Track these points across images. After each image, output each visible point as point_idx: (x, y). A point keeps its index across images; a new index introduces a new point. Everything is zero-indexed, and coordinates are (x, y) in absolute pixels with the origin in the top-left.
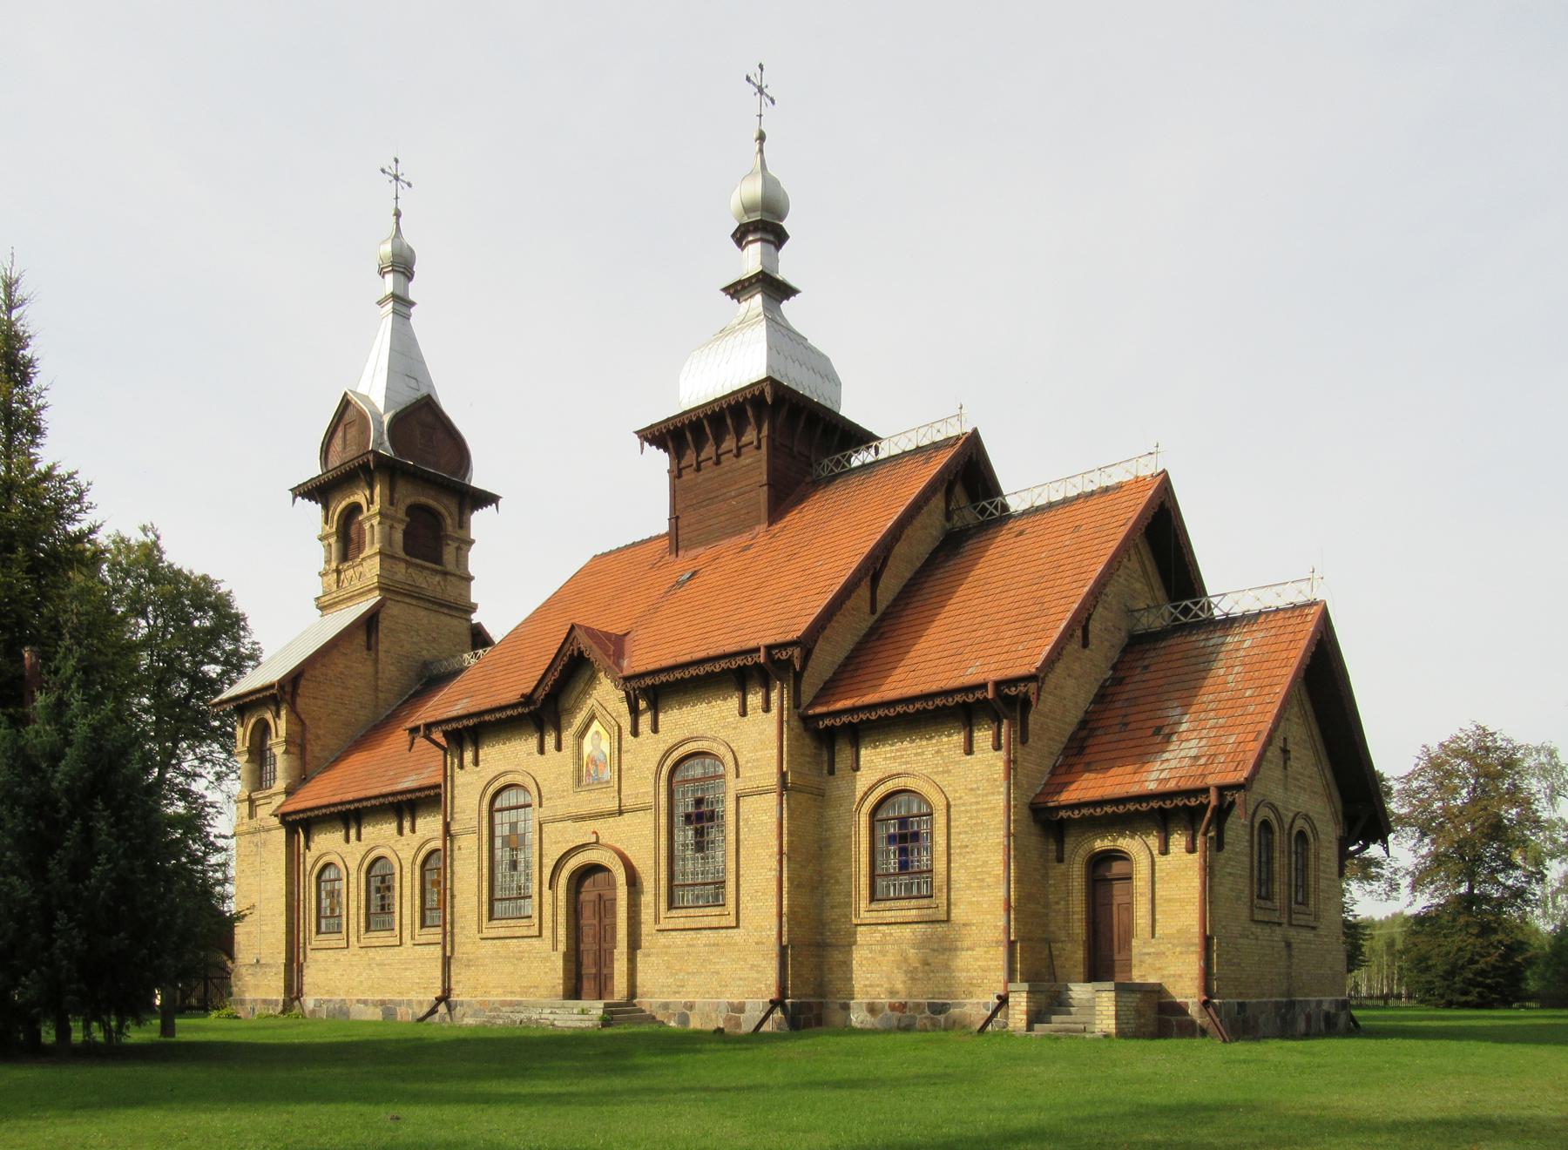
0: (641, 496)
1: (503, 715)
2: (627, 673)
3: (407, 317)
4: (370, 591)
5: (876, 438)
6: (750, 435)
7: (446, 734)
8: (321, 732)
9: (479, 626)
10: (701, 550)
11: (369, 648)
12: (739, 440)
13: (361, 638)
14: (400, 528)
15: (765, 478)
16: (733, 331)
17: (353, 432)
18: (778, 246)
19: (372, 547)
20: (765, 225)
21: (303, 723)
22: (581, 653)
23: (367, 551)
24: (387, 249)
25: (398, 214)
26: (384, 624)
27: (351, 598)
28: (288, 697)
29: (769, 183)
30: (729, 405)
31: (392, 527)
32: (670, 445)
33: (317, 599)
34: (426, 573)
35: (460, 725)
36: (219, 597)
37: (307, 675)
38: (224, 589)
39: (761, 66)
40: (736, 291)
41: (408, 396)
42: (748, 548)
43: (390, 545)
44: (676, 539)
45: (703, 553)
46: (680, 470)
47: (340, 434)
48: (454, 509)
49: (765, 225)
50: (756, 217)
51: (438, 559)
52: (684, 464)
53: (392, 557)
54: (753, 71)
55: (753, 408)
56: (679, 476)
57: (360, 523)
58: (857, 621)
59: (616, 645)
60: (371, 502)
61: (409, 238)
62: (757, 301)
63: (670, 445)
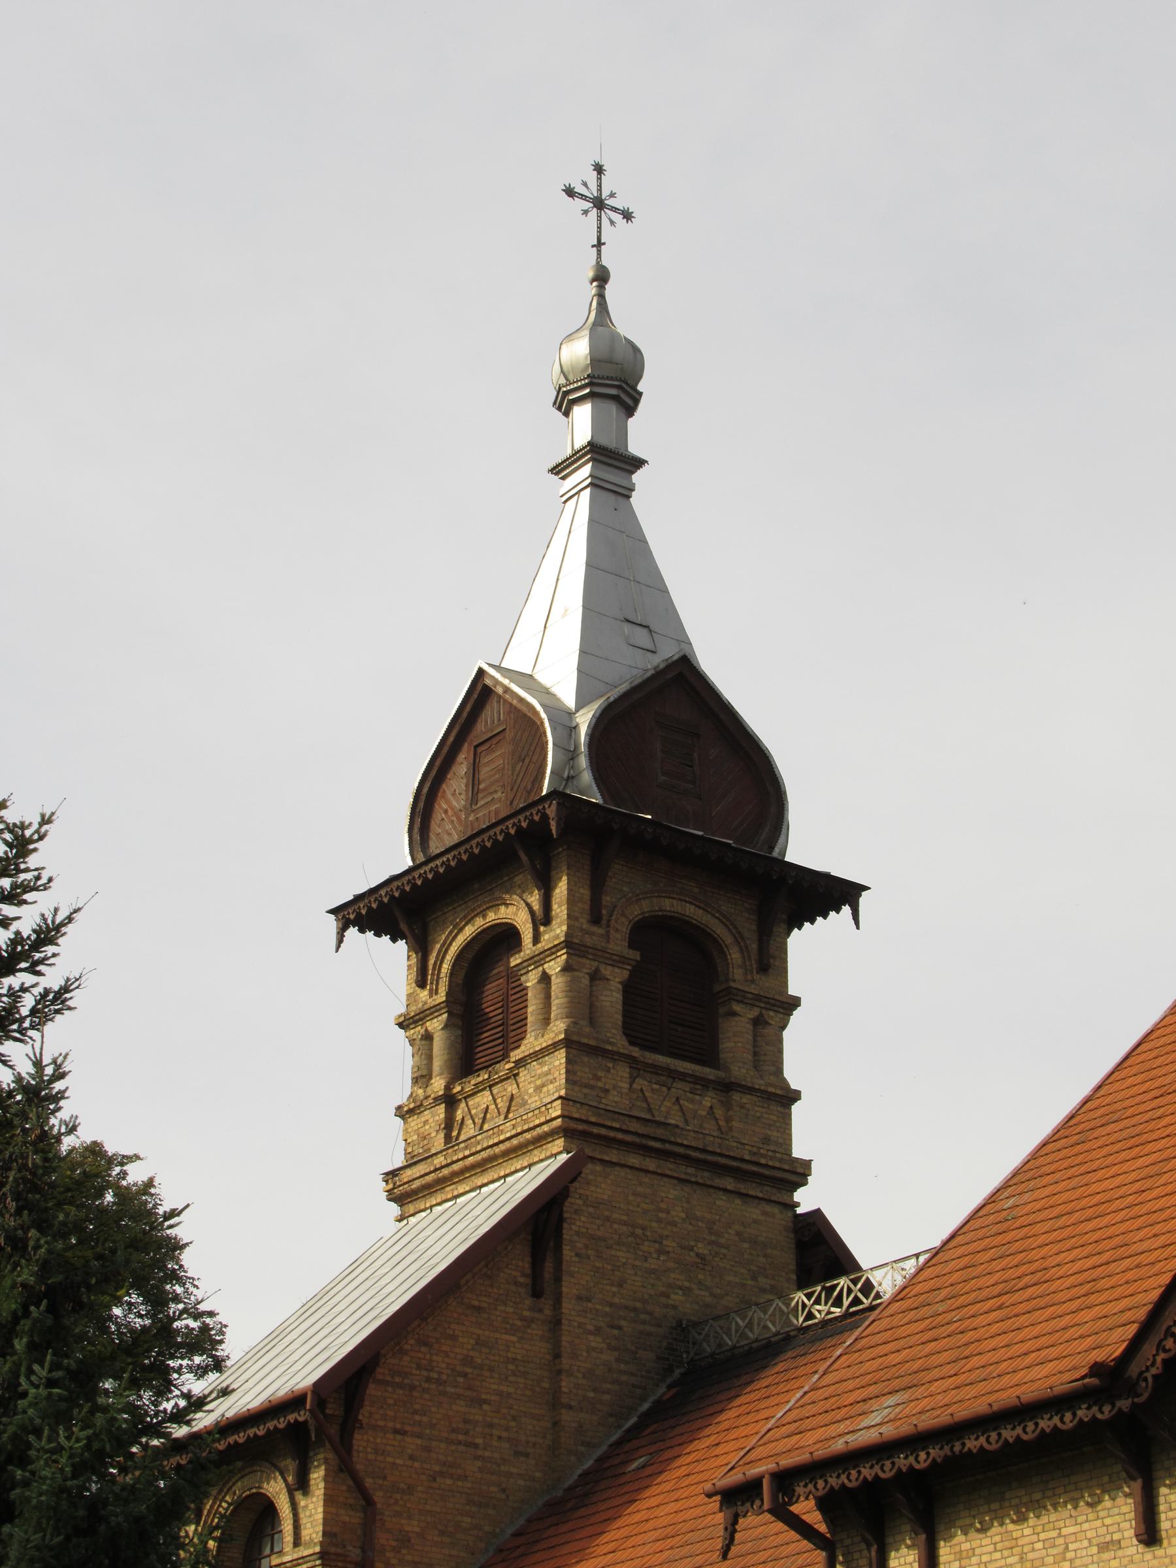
1: (1028, 1431)
3: (625, 493)
4: (540, 1141)
7: (824, 1504)
8: (413, 1526)
9: (817, 1216)
11: (537, 1293)
13: (517, 1265)
14: (616, 976)
17: (495, 762)
18: (630, 410)
19: (544, 1032)
21: (369, 1502)
23: (532, 1042)
24: (579, 350)
25: (601, 277)
26: (577, 1224)
27: (482, 1166)
28: (333, 1430)
31: (595, 976)
32: (403, 927)
33: (390, 1175)
34: (679, 1087)
35: (886, 1470)
36: (125, 1195)
37: (381, 1372)
38: (135, 1175)
41: (632, 666)
43: (592, 1021)
47: (461, 768)
48: (749, 928)
51: (708, 1054)
53: (597, 1051)
57: (514, 976)
60: (543, 919)
61: (625, 324)
63: (403, 927)
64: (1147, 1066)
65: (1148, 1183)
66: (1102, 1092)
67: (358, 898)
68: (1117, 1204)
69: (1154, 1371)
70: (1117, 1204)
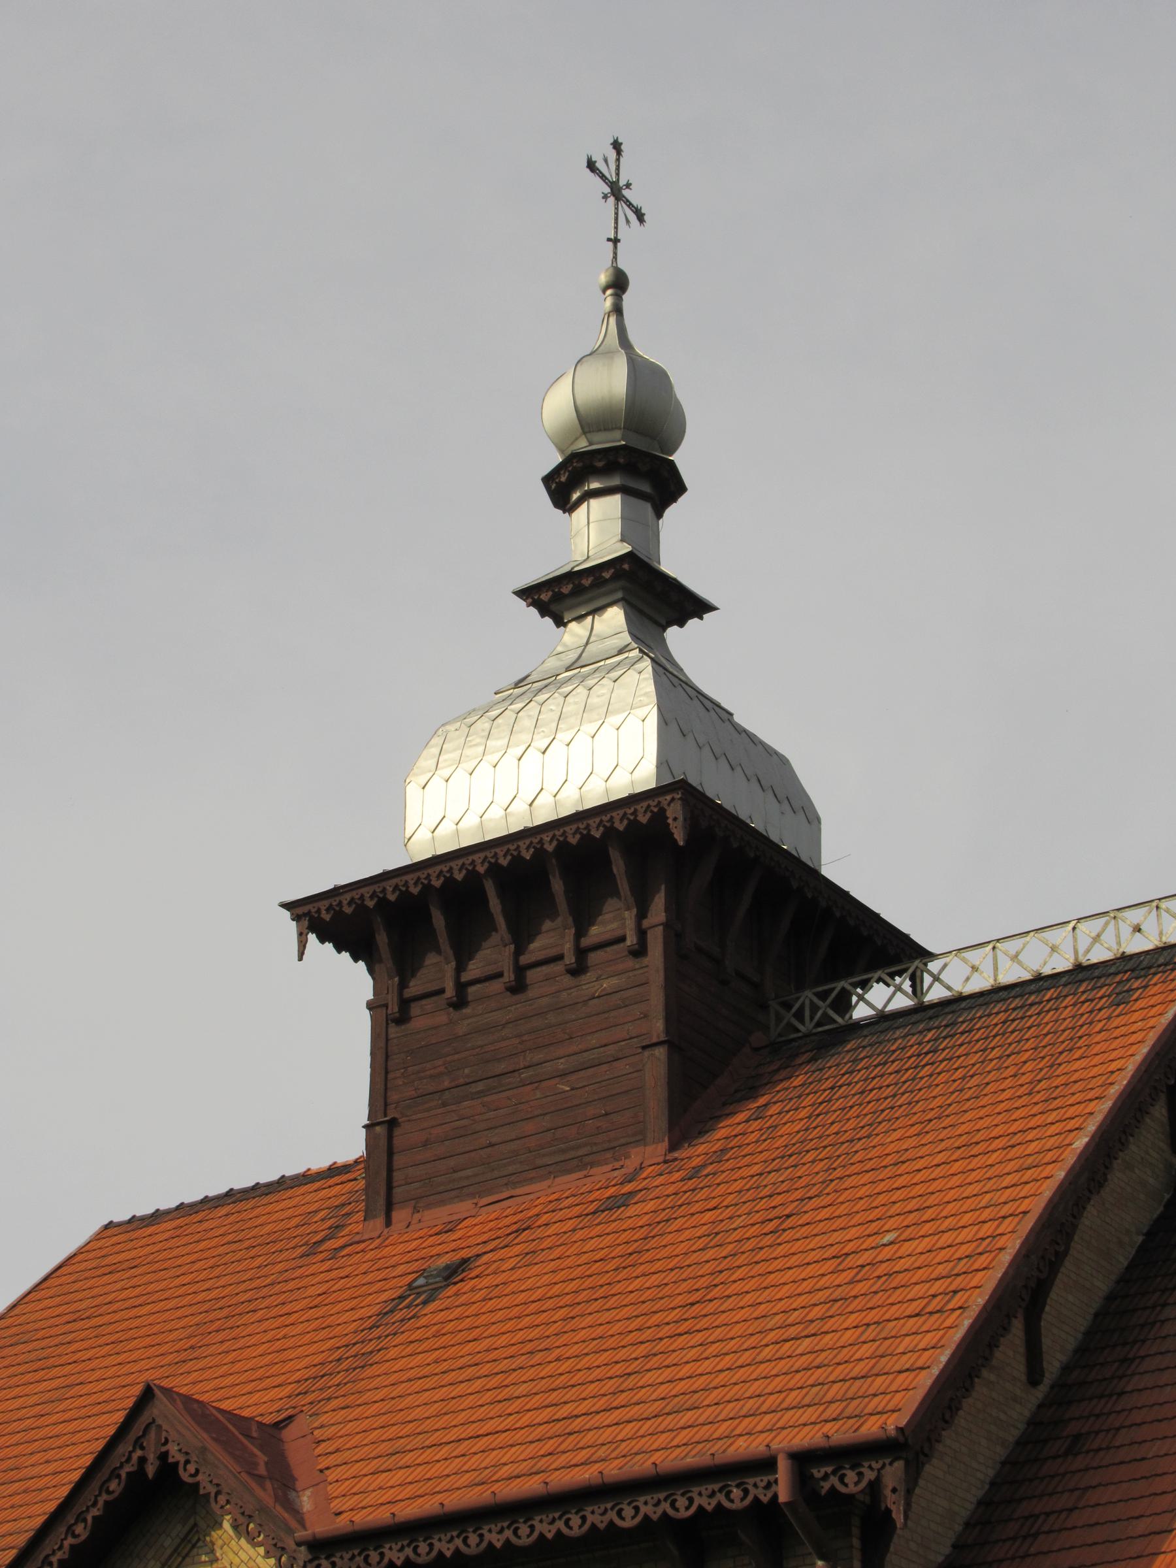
0: (293, 1074)
2: (321, 1527)
5: (926, 955)
6: (615, 919)
10: (463, 1207)
12: (580, 933)
15: (658, 1028)
16: (551, 682)
20: (629, 454)
22: (168, 1469)
29: (648, 381)
30: (563, 846)
32: (382, 939)
39: (617, 146)
40: (558, 598)
42: (624, 1201)
44: (390, 1171)
45: (475, 1223)
46: (405, 1004)
49: (629, 454)
50: (603, 441)
52: (416, 987)
54: (602, 151)
55: (502, 892)
56: (402, 1018)
58: (1006, 1404)
59: (265, 1447)
62: (613, 620)
63: (382, 939)
64: (66, 1289)
65: (47, 1408)
66: (16, 1311)
67: (336, 891)
68: (14, 1426)
69: (59, 1555)
70: (14, 1426)
